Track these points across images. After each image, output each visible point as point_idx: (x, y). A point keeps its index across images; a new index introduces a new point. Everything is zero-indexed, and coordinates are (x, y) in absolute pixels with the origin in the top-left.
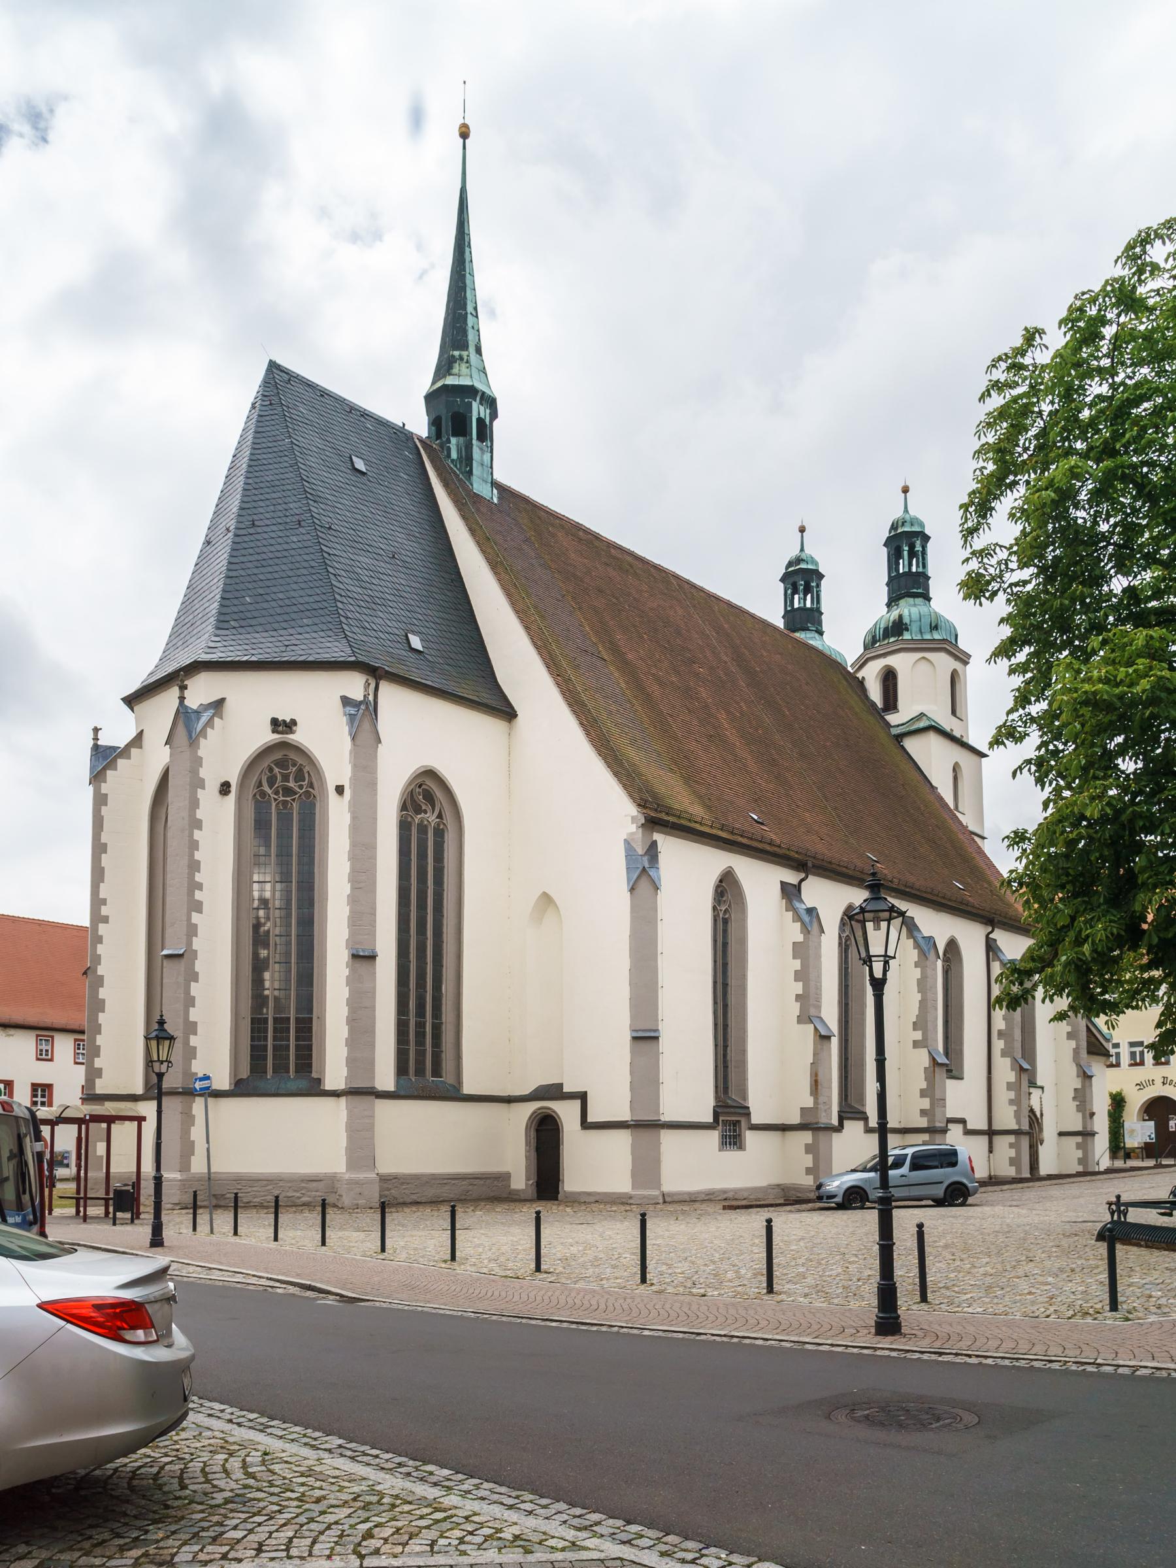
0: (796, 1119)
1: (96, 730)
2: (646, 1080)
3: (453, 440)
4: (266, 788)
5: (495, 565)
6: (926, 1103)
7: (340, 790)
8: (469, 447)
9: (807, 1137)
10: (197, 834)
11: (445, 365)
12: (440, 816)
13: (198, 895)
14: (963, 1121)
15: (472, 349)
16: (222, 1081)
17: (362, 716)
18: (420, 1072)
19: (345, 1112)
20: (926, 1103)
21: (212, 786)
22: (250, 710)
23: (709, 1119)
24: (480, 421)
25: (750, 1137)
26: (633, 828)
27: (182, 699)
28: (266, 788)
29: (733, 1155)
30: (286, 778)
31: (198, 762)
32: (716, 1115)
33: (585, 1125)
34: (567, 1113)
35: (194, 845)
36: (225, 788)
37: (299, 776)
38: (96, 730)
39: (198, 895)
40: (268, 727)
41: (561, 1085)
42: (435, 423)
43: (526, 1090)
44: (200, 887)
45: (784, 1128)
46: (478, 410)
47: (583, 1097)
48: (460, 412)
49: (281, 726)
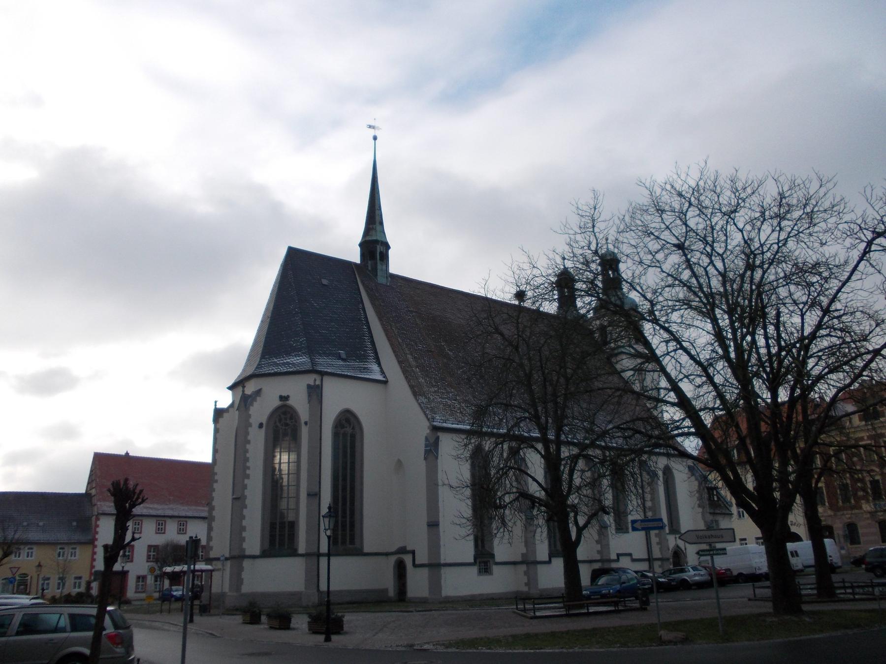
0: (519, 559)
1: (216, 402)
2: (434, 545)
3: (370, 262)
4: (278, 424)
5: (380, 319)
6: (599, 547)
7: (306, 423)
8: (376, 264)
9: (523, 568)
10: (248, 446)
11: (368, 231)
12: (353, 428)
13: (248, 472)
14: (630, 555)
15: (377, 223)
16: (257, 552)
17: (315, 393)
18: (344, 543)
19: (546, 543)
20: (599, 547)
21: (255, 425)
22: (272, 392)
23: (472, 560)
24: (381, 253)
25: (495, 569)
26: (428, 431)
27: (243, 391)
28: (278, 424)
29: (486, 578)
30: (286, 419)
31: (250, 416)
32: (475, 559)
33: (415, 565)
34: (408, 559)
35: (246, 451)
36: (261, 425)
37: (291, 418)
38: (216, 402)
39: (248, 472)
40: (278, 398)
41: (405, 547)
42: (363, 255)
43: (393, 550)
44: (249, 468)
45: (514, 563)
46: (379, 248)
47: (413, 553)
48: (374, 246)
49: (282, 398)
